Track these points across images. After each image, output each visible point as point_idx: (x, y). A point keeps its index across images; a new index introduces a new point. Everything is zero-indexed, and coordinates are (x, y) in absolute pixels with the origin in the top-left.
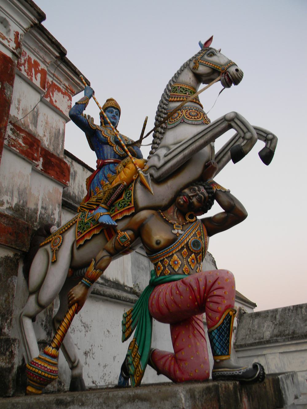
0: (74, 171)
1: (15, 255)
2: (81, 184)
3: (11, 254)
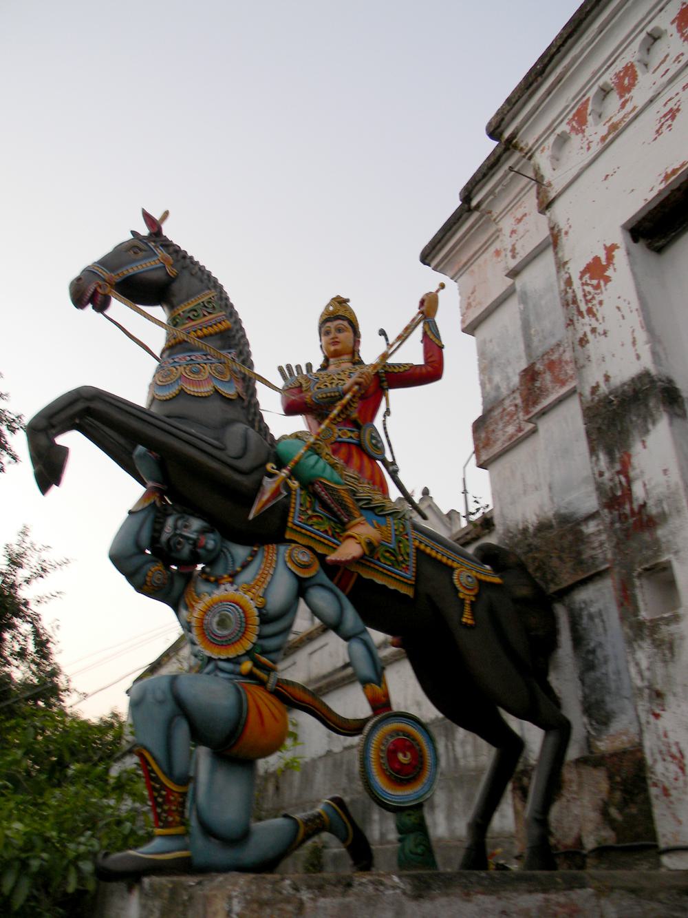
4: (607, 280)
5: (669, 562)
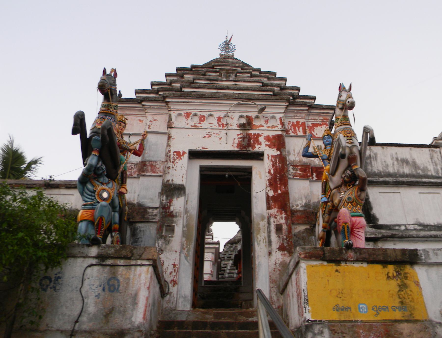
0: (375, 154)
1: (310, 226)
2: (383, 161)
3: (308, 227)
4: (181, 159)
5: (174, 226)
